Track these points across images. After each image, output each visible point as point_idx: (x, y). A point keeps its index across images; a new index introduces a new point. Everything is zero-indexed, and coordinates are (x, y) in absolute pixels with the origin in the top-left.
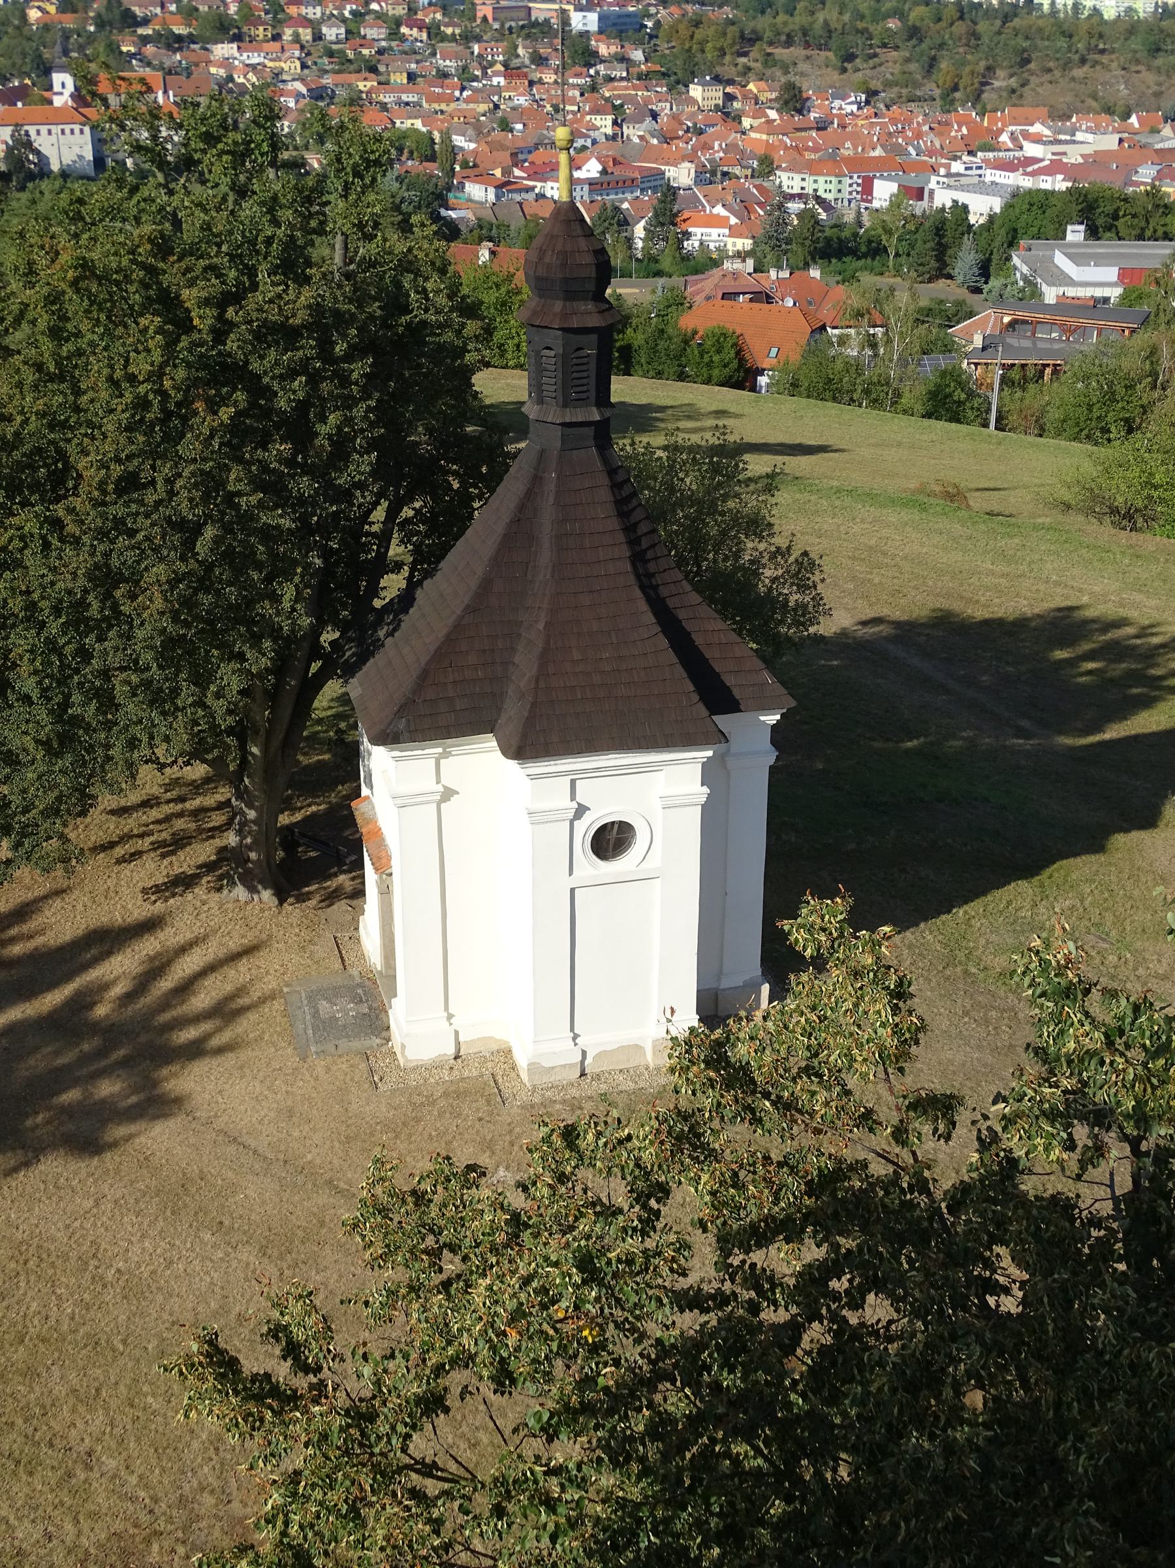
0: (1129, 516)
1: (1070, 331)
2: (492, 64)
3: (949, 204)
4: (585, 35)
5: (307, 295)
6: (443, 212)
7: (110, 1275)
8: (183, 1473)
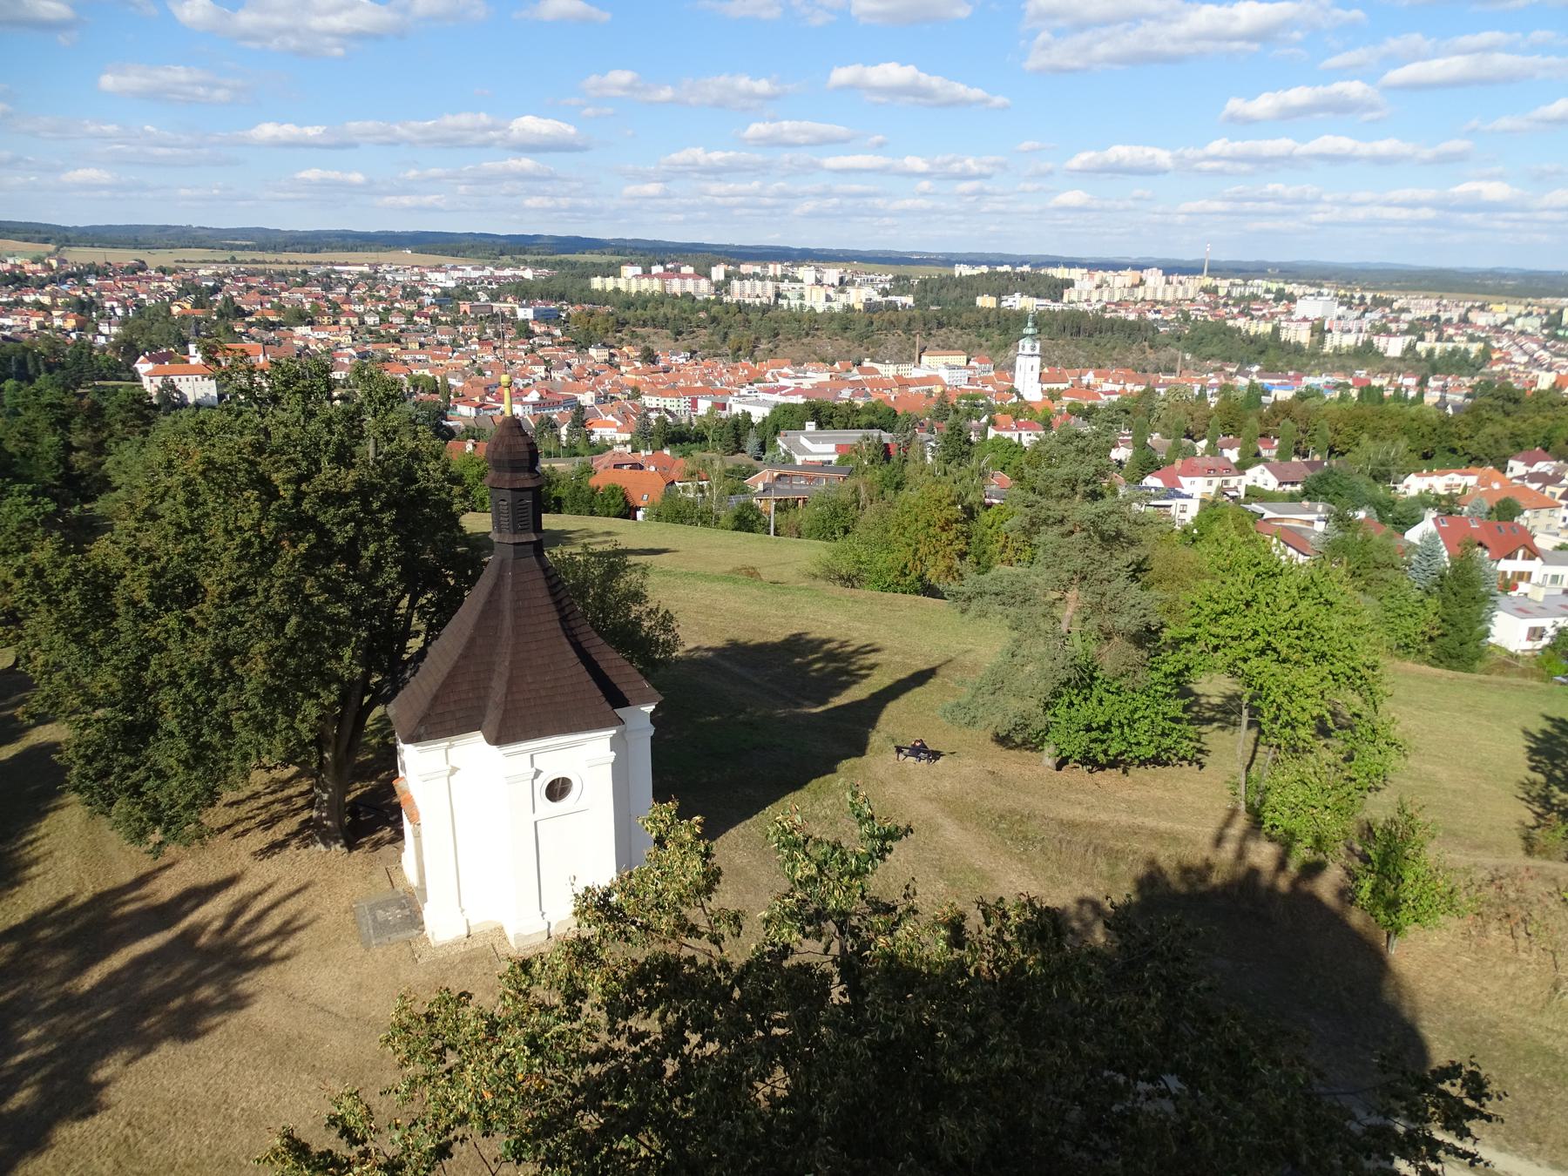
0: (849, 580)
1: (812, 479)
2: (471, 338)
4: (526, 321)
6: (444, 423)
7: (236, 1112)
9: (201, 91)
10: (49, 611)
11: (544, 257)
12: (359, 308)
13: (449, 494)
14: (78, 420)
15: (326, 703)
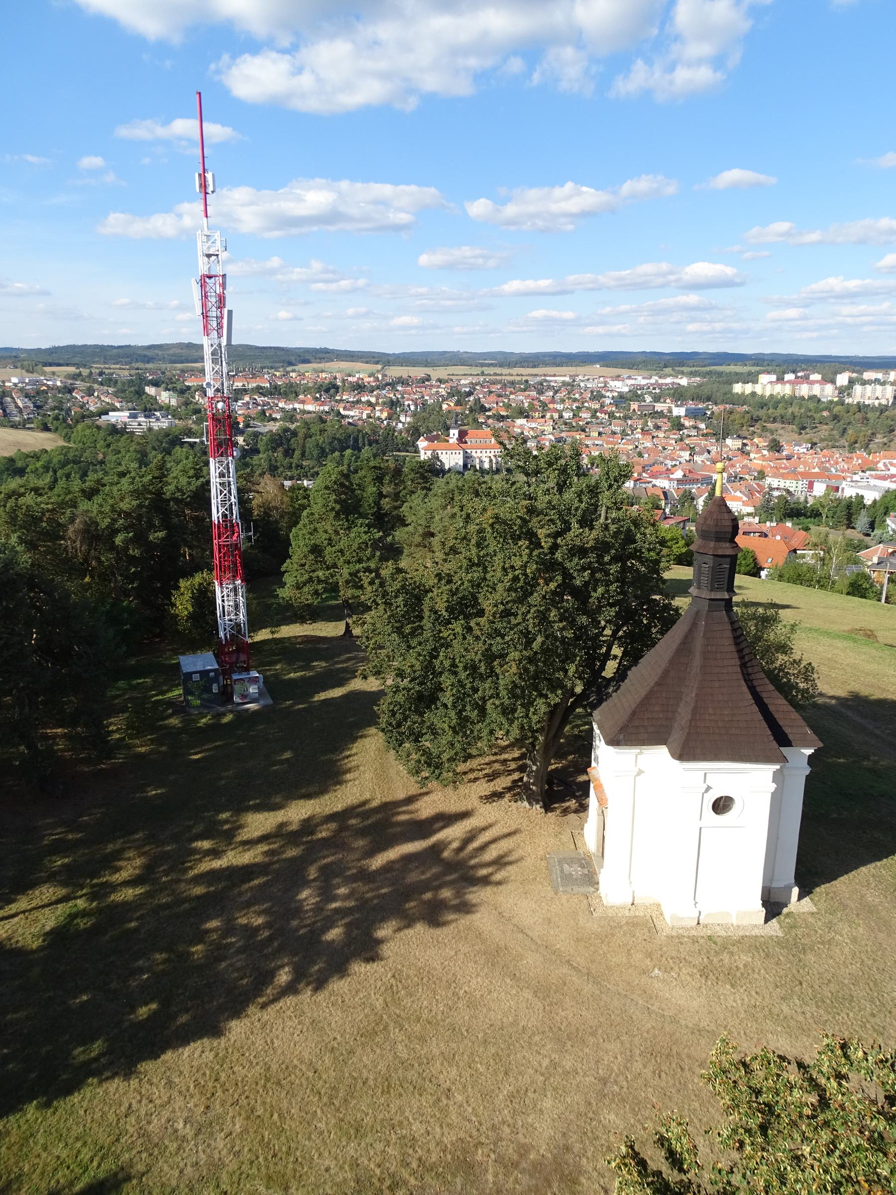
2: (636, 429)
3: (854, 495)
4: (679, 417)
5: (594, 533)
8: (494, 1111)
9: (480, 261)
10: (385, 610)
11: (697, 369)
12: (560, 407)
13: (658, 554)
14: (387, 478)
15: (552, 703)
